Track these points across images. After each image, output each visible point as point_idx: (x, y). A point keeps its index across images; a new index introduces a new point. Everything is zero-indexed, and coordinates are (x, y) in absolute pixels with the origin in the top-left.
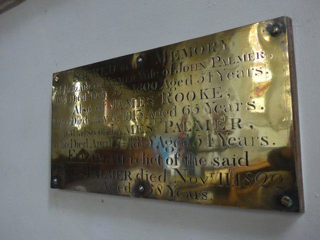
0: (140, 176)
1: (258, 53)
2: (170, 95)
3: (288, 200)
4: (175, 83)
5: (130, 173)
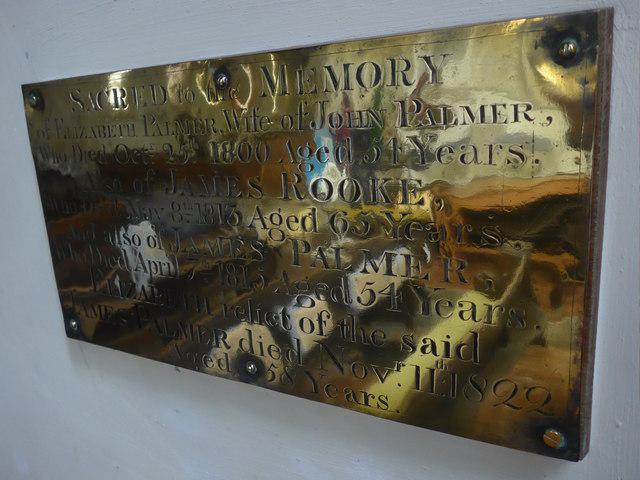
0: (246, 345)
1: (516, 107)
2: (300, 180)
3: (556, 438)
4: (311, 152)
5: (225, 337)
